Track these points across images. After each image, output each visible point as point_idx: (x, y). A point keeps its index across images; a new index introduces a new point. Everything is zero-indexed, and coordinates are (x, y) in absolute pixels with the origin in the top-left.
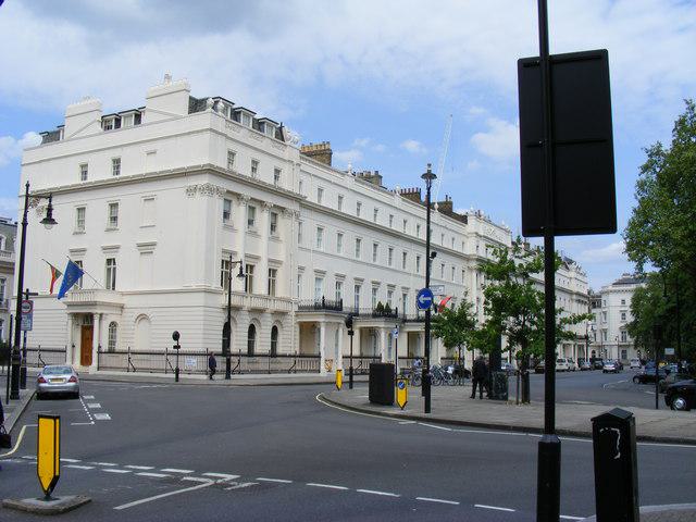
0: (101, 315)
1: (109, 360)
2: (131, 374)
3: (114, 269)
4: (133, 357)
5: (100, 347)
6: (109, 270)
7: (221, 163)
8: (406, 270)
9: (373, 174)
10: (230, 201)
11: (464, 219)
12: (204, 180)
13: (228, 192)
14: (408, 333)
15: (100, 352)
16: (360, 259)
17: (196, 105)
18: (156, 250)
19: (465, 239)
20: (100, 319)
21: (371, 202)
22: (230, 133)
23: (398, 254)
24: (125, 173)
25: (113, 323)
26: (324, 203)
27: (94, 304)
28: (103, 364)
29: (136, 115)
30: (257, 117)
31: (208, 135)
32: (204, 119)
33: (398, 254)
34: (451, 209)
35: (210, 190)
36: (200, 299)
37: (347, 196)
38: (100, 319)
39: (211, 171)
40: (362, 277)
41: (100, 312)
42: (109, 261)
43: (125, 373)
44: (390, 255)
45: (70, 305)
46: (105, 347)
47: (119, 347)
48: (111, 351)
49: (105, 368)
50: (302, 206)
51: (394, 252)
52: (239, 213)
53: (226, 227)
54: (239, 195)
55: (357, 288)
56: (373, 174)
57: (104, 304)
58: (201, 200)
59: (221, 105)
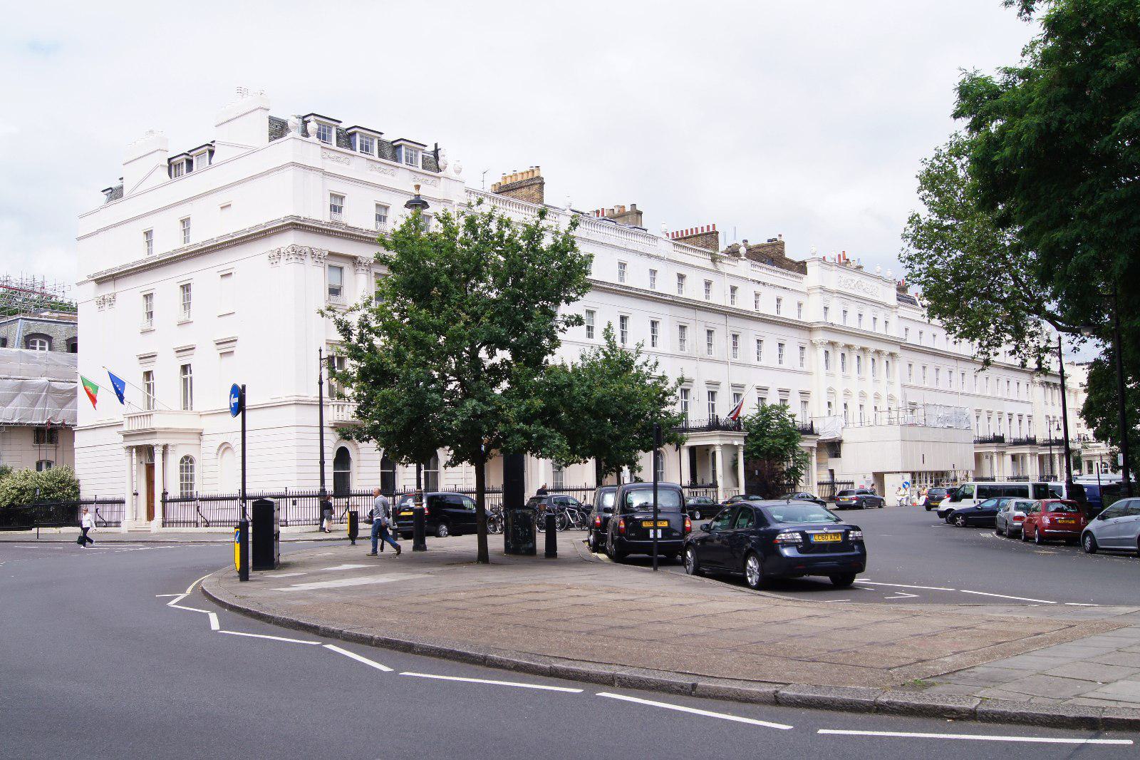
0: (165, 447)
1: (176, 511)
2: (202, 529)
3: (191, 378)
4: (203, 505)
5: (165, 494)
6: (185, 380)
7: (321, 214)
8: (714, 356)
9: (628, 209)
10: (341, 269)
11: (801, 268)
12: (289, 240)
13: (331, 254)
14: (692, 450)
15: (164, 501)
16: (784, 366)
17: (278, 129)
18: (238, 348)
19: (802, 299)
20: (164, 454)
21: (644, 259)
22: (331, 166)
23: (770, 348)
24: (199, 237)
25: (187, 457)
26: (660, 288)
27: (152, 433)
28: (171, 517)
29: (187, 160)
30: (344, 126)
31: (290, 173)
32: (290, 146)
33: (770, 348)
34: (782, 253)
35: (299, 254)
36: (291, 415)
37: (893, 319)
38: (164, 454)
39: (297, 225)
40: (740, 383)
41: (164, 442)
42: (185, 368)
43: (192, 529)
44: (653, 331)
45: (127, 436)
46: (174, 492)
47: (200, 489)
48: (186, 499)
49: (172, 523)
50: (902, 348)
51: (764, 346)
52: (836, 357)
53: (860, 379)
54: (355, 258)
55: (712, 395)
56: (628, 209)
57: (167, 431)
58: (288, 269)
59: (312, 127)
